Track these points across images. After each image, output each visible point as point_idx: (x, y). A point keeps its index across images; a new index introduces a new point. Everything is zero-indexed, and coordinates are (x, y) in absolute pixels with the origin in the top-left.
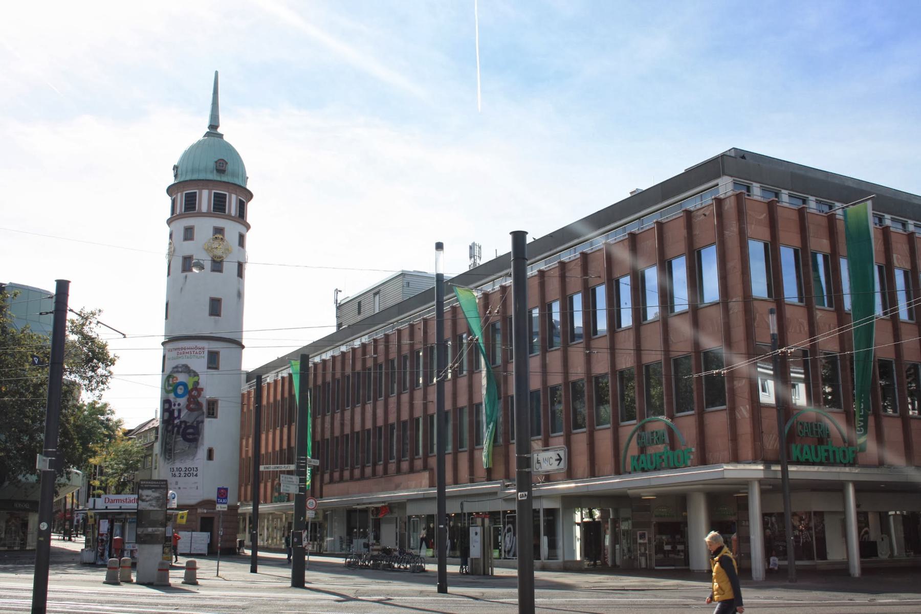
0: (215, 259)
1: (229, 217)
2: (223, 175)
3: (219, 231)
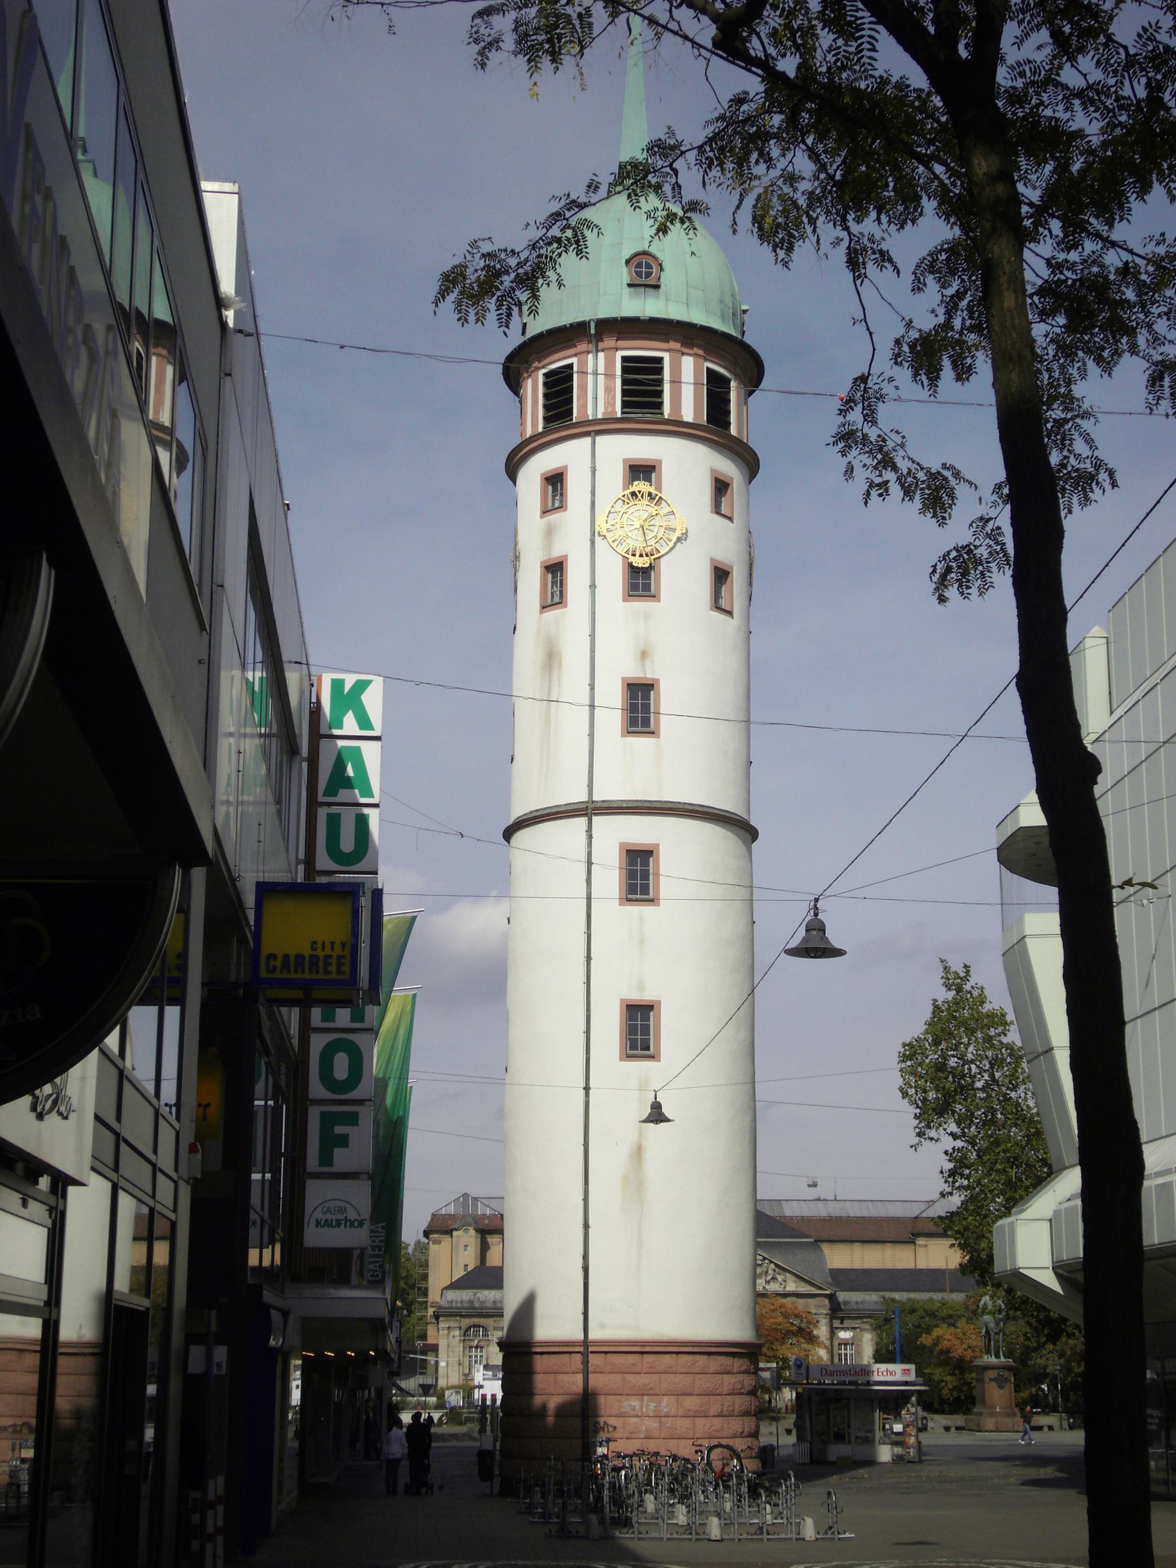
1: (678, 429)
3: (641, 471)
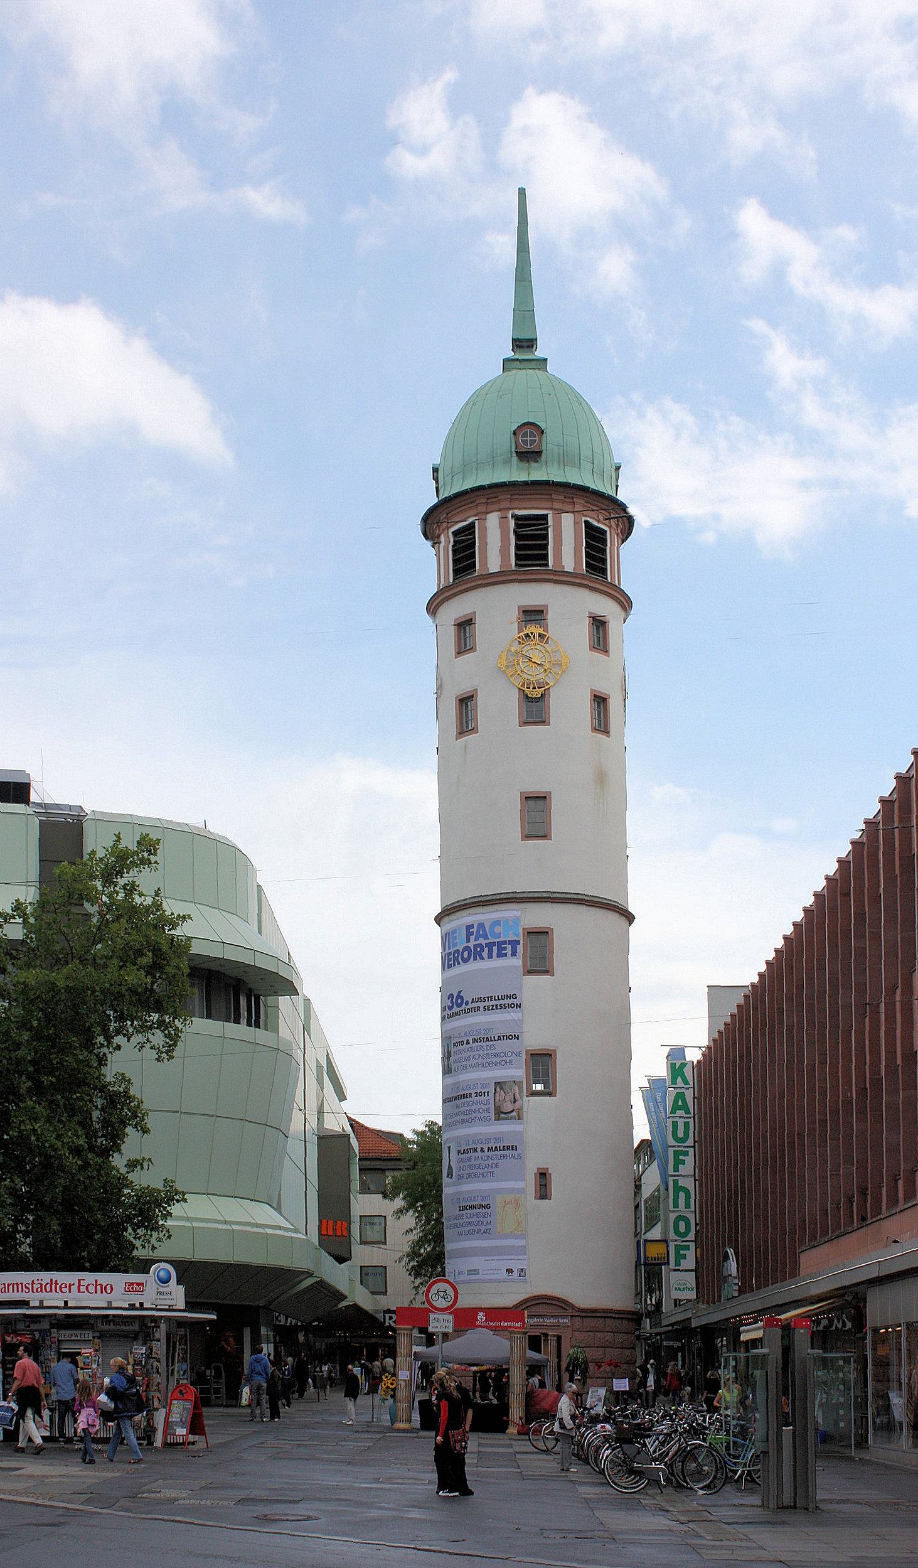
0: (528, 692)
1: (561, 578)
2: (533, 464)
3: (533, 615)
